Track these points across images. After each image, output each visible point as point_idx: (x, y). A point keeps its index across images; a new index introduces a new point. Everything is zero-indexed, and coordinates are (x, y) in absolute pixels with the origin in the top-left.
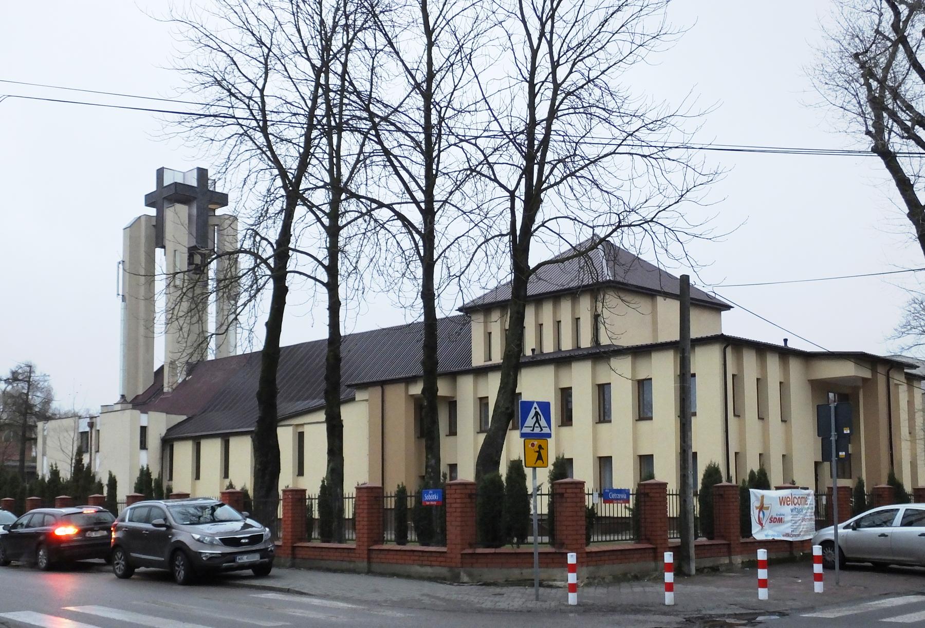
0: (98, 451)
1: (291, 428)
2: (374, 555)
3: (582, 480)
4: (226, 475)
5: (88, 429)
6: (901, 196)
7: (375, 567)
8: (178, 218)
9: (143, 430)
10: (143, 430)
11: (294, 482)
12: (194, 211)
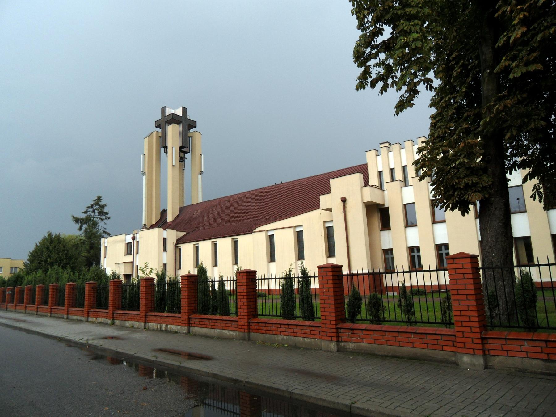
0: (138, 253)
1: (264, 233)
2: (27, 308)
3: (341, 265)
4: (236, 263)
5: (132, 241)
6: (298, 178)
7: (27, 311)
8: (173, 131)
9: (165, 239)
10: (165, 239)
11: (327, 260)
12: (181, 129)
